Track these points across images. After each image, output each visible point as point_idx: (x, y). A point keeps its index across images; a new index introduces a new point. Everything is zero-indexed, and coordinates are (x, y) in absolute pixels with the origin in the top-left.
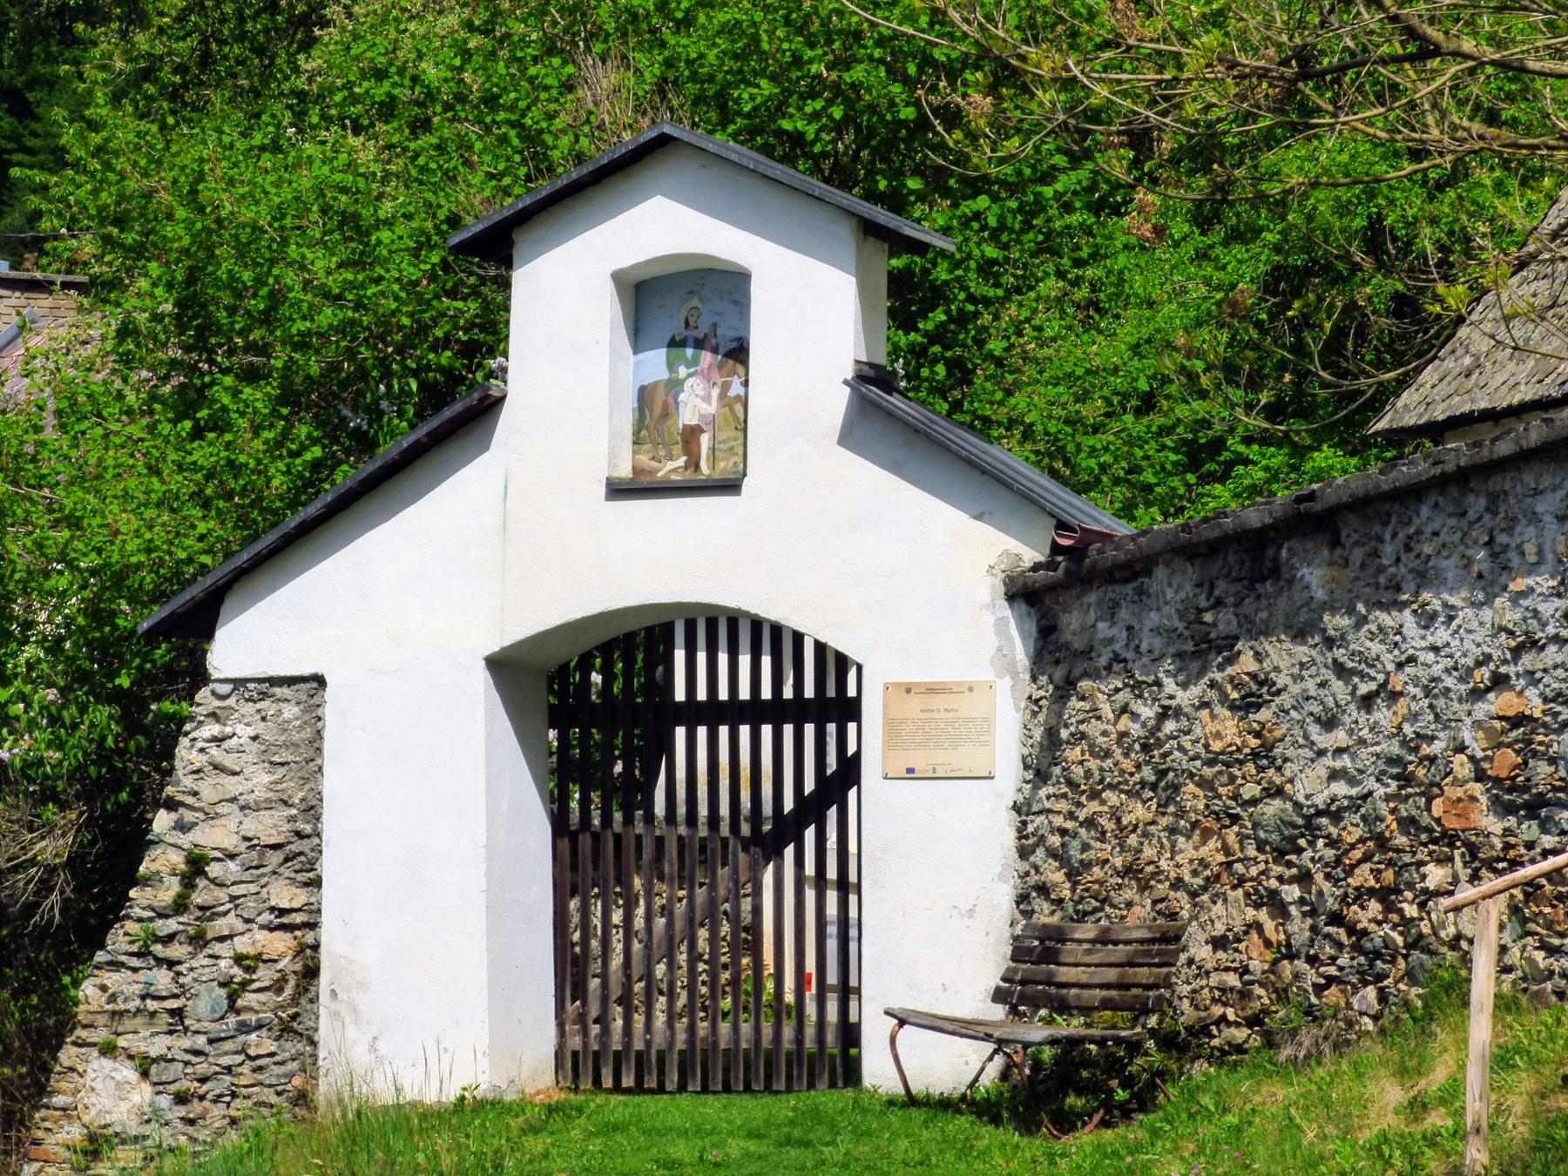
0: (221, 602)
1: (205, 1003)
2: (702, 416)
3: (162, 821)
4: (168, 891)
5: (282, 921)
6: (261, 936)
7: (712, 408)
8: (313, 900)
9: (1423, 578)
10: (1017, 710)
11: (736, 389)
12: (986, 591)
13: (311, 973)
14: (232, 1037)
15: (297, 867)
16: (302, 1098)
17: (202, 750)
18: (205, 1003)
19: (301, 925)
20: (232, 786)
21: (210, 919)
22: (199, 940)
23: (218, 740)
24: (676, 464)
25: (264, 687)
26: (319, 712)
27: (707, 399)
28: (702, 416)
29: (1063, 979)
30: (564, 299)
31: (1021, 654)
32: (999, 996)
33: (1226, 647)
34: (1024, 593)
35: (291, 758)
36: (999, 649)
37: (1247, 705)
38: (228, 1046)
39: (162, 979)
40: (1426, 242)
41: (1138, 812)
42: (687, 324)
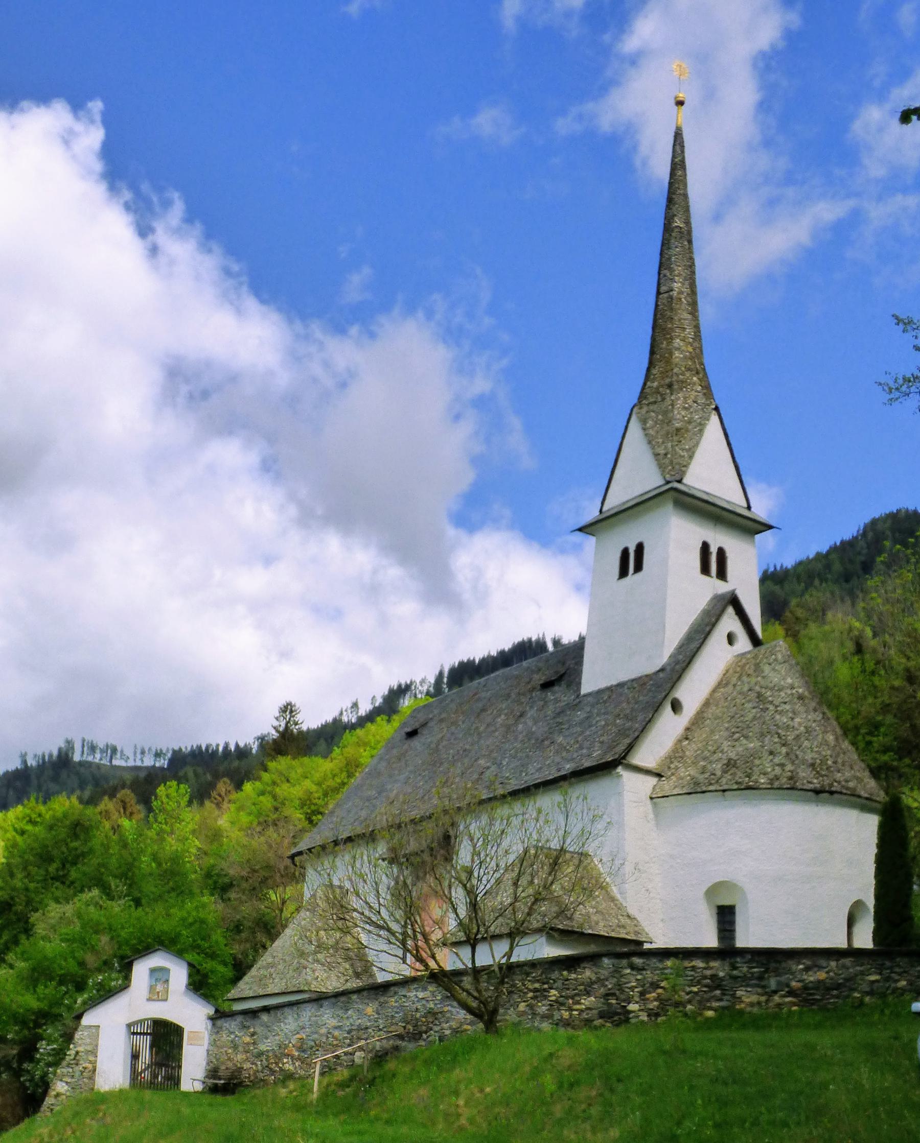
1: (77, 1074)
3: (72, 1046)
4: (72, 1057)
5: (90, 1062)
9: (285, 1018)
13: (95, 1070)
16: (93, 1089)
18: (77, 1074)
19: (94, 1063)
22: (77, 1064)
24: (155, 996)
30: (141, 970)
31: (209, 1027)
33: (249, 1027)
34: (212, 1019)
37: (253, 1035)
39: (71, 1070)
40: (20, 998)
41: (230, 1051)
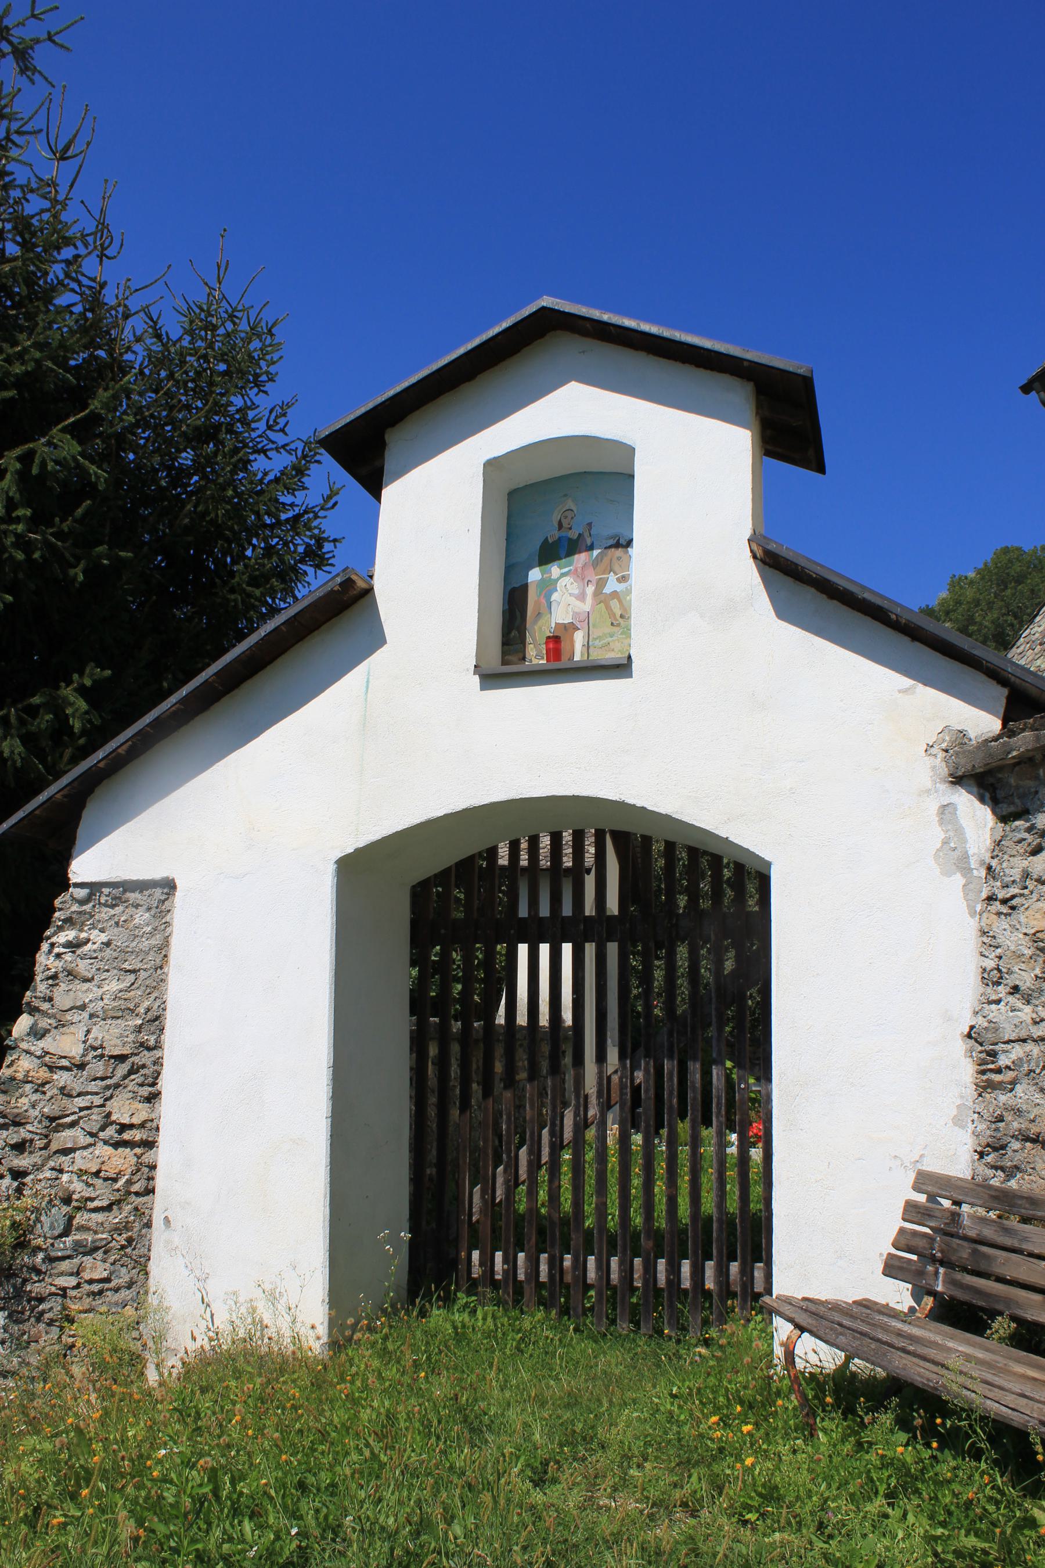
0: (82, 806)
2: (576, 614)
6: (103, 1151)
7: (587, 606)
8: (153, 1116)
10: (972, 913)
11: (612, 585)
12: (924, 772)
14: (69, 1257)
15: (140, 1080)
17: (58, 956)
20: (85, 993)
21: (56, 1130)
23: (73, 946)
25: (116, 892)
26: (168, 918)
27: (582, 597)
28: (576, 614)
29: (1009, 1273)
32: (892, 1269)
35: (139, 966)
36: (945, 842)
38: (65, 1266)
42: (560, 525)
